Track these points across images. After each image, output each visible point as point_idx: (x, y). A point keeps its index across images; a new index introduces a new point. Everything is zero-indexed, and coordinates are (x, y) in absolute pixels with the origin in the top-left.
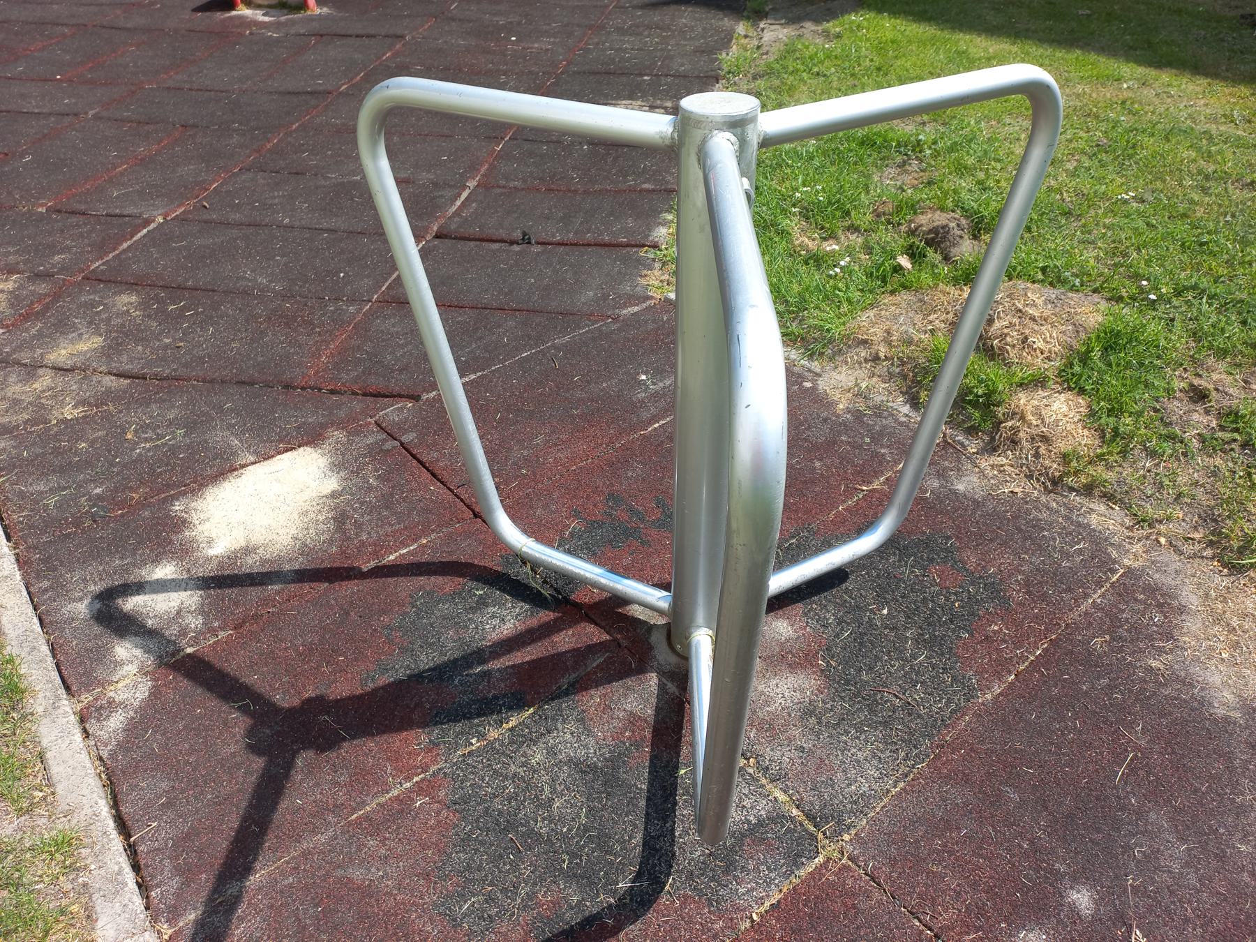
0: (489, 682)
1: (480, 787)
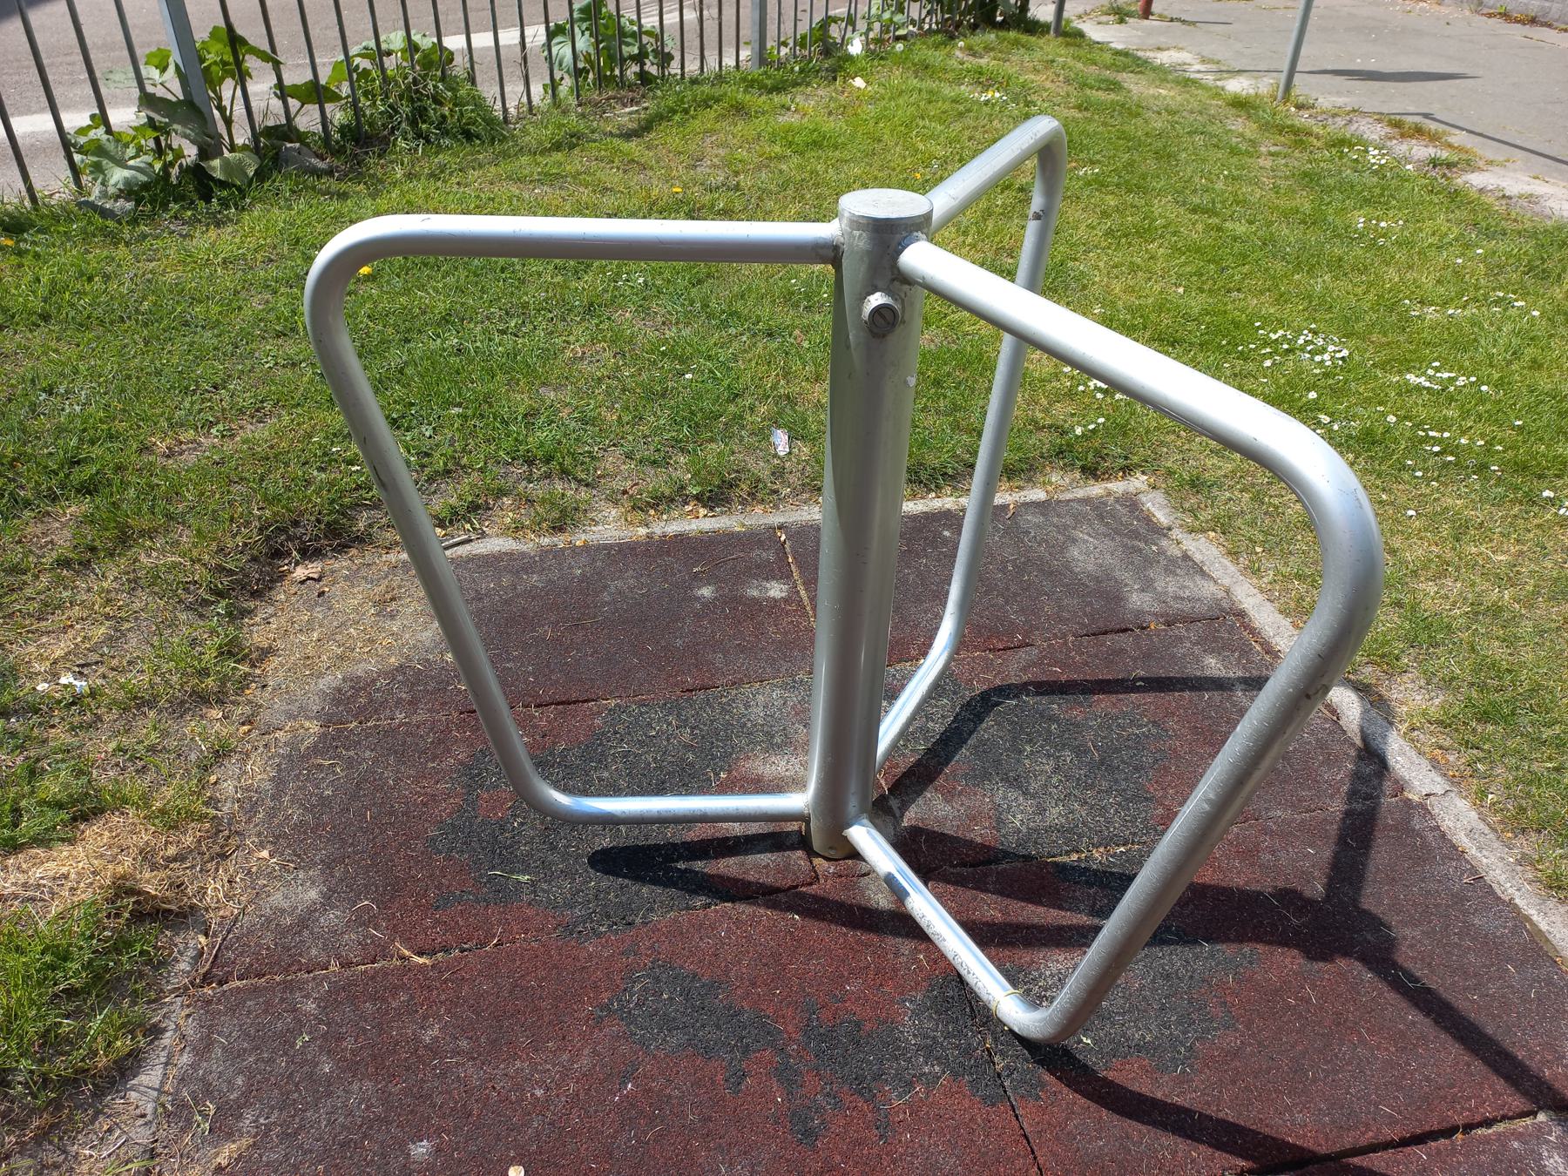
0: (1095, 904)
1: (1119, 805)
